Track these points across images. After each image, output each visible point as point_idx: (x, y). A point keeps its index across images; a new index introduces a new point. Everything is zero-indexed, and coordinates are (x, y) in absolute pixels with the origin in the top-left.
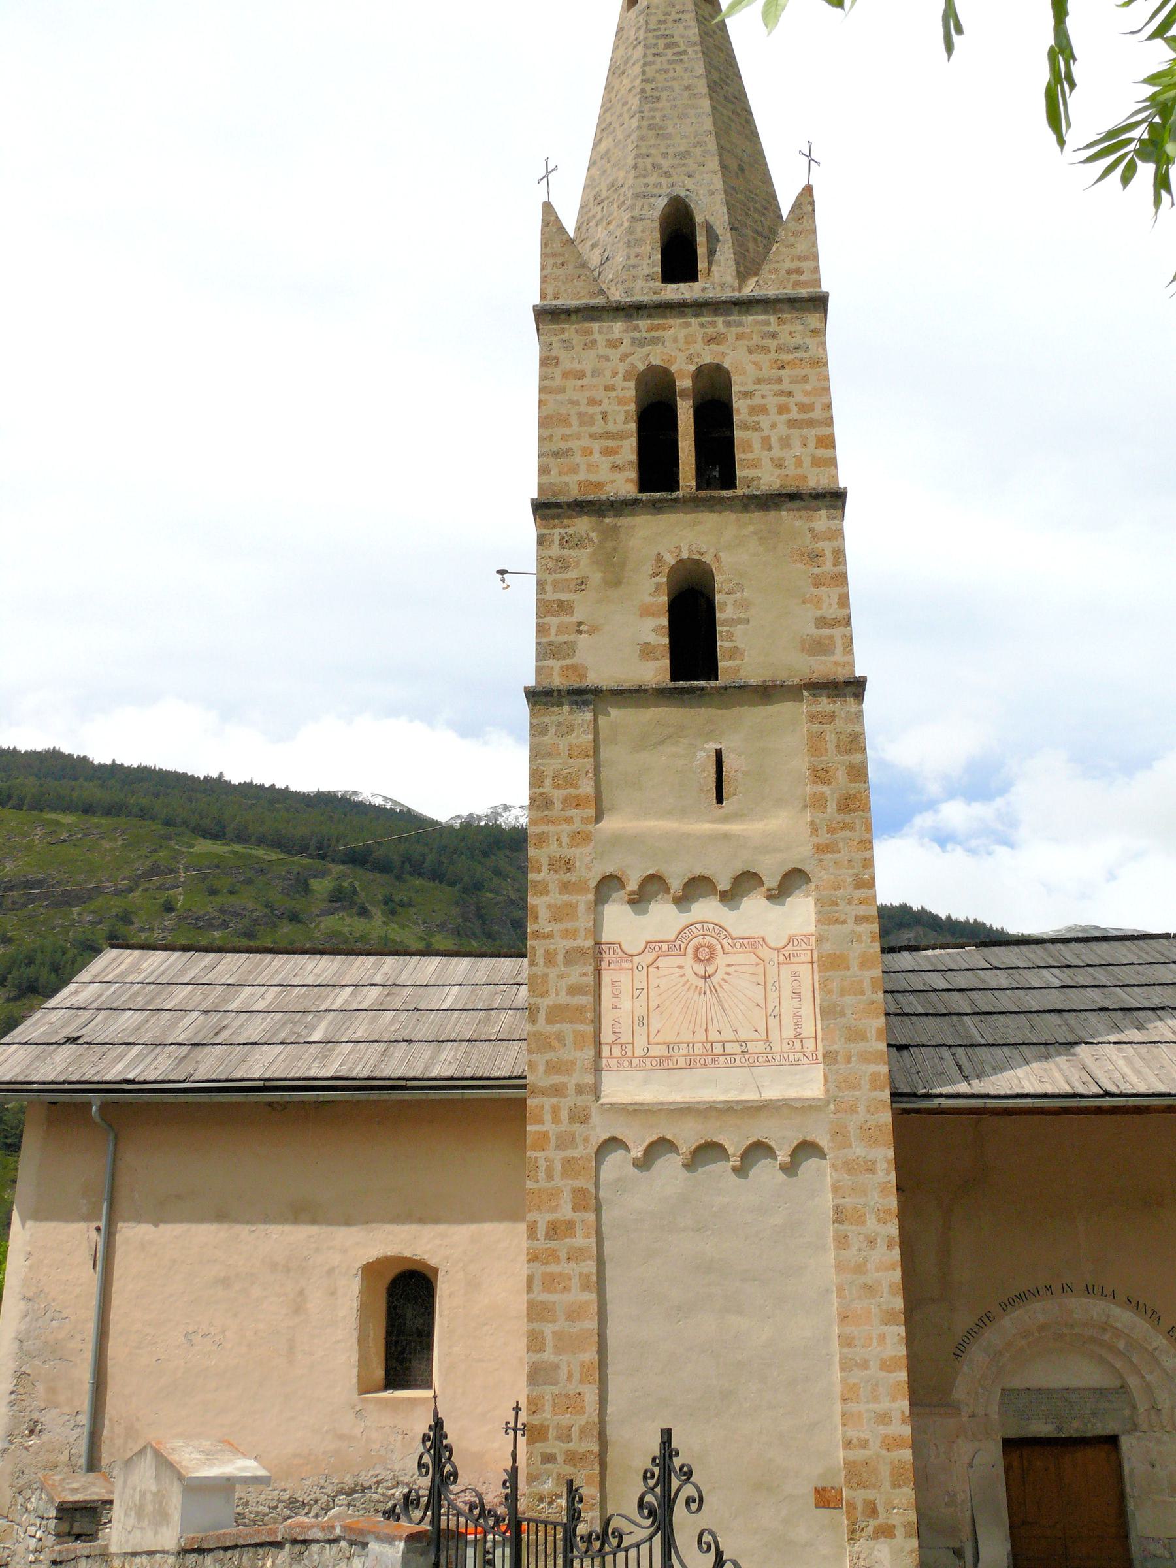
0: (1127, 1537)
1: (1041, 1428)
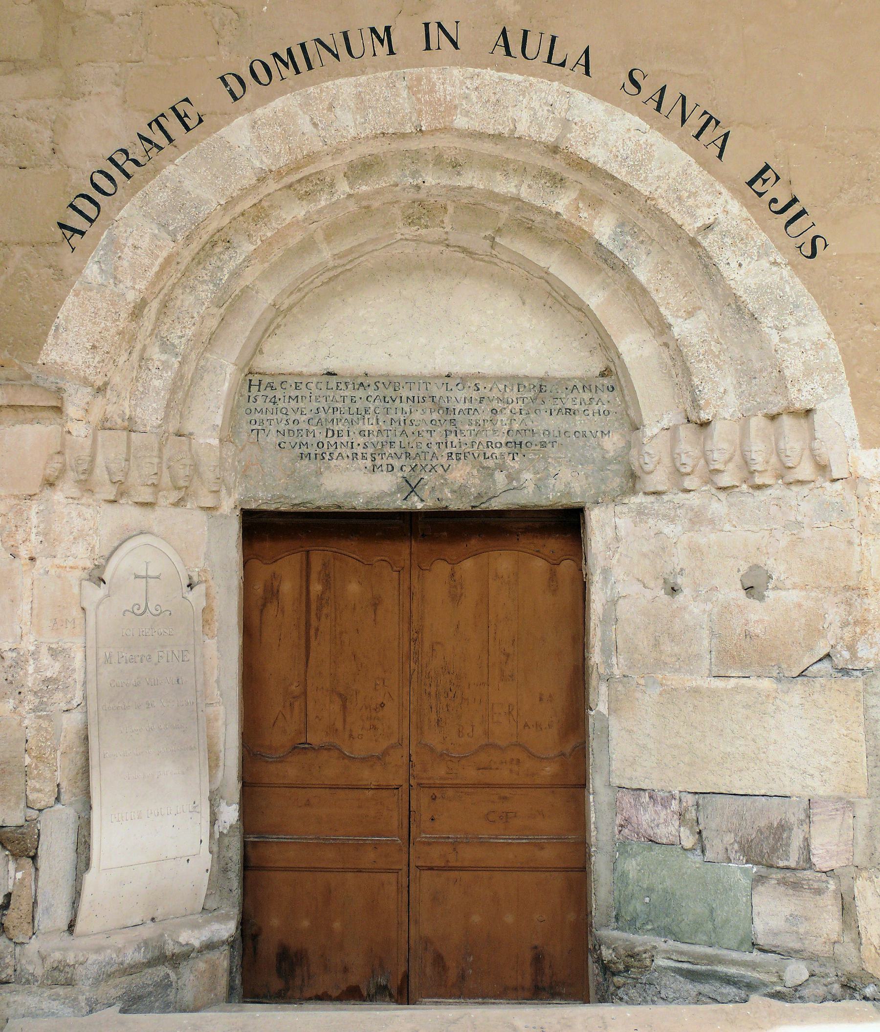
0: (581, 785)
1: (357, 484)
